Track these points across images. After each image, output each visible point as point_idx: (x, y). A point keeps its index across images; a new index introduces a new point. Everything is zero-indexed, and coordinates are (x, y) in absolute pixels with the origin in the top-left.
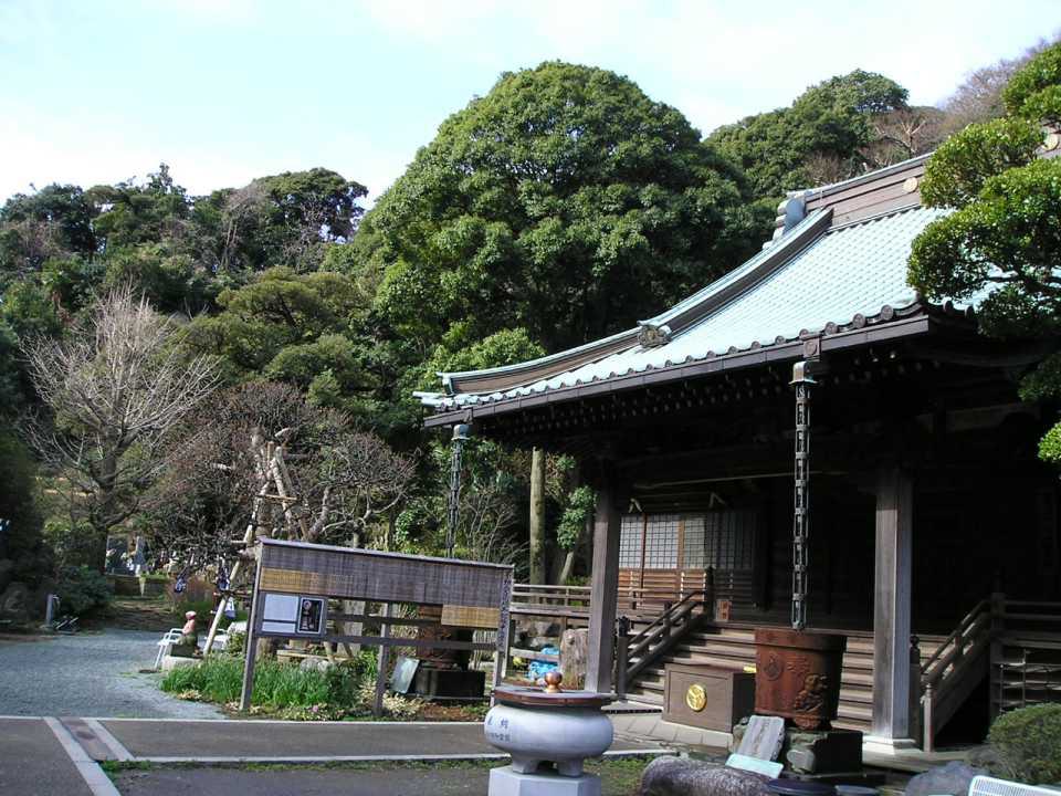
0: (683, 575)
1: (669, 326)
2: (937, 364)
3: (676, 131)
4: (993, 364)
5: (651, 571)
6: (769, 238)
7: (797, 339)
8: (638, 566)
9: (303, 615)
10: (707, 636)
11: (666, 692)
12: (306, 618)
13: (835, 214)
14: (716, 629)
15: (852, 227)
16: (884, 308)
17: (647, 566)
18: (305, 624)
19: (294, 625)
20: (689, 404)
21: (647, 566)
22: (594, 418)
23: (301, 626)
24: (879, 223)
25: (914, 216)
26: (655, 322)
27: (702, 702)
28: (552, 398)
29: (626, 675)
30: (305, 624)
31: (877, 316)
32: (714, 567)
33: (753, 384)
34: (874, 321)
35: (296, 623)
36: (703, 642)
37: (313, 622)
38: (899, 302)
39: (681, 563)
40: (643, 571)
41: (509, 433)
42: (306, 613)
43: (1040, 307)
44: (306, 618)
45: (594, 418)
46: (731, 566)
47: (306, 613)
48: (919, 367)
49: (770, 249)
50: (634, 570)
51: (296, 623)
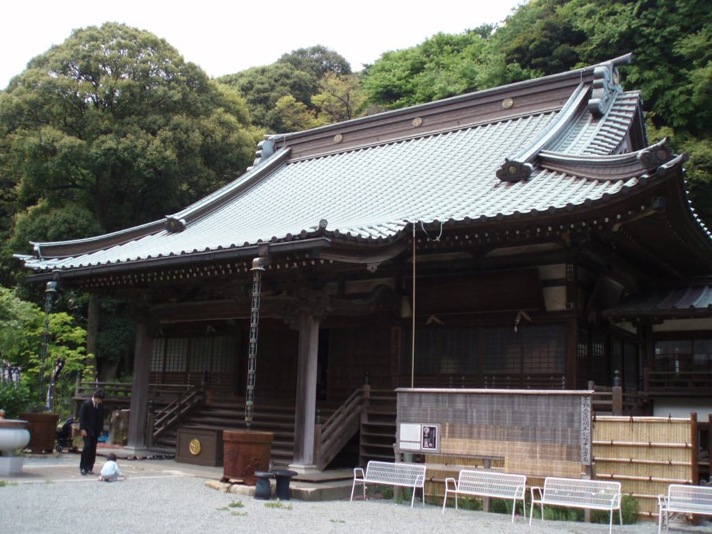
0: (189, 375)
1: (185, 219)
2: (331, 262)
3: (195, 78)
4: (362, 262)
5: (169, 373)
7: (256, 244)
8: (161, 370)
11: (177, 446)
13: (293, 152)
14: (208, 408)
17: (167, 370)
18: (426, 443)
20: (195, 275)
21: (167, 370)
22: (137, 281)
24: (318, 160)
26: (176, 216)
27: (199, 449)
28: (111, 269)
29: (153, 437)
30: (426, 443)
31: (299, 236)
32: (209, 370)
34: (297, 238)
36: (201, 416)
37: (431, 442)
38: (311, 228)
39: (188, 368)
40: (164, 372)
43: (641, 28)
45: (137, 281)
46: (219, 370)
48: (322, 262)
49: (252, 172)
50: (159, 373)
51: (420, 442)
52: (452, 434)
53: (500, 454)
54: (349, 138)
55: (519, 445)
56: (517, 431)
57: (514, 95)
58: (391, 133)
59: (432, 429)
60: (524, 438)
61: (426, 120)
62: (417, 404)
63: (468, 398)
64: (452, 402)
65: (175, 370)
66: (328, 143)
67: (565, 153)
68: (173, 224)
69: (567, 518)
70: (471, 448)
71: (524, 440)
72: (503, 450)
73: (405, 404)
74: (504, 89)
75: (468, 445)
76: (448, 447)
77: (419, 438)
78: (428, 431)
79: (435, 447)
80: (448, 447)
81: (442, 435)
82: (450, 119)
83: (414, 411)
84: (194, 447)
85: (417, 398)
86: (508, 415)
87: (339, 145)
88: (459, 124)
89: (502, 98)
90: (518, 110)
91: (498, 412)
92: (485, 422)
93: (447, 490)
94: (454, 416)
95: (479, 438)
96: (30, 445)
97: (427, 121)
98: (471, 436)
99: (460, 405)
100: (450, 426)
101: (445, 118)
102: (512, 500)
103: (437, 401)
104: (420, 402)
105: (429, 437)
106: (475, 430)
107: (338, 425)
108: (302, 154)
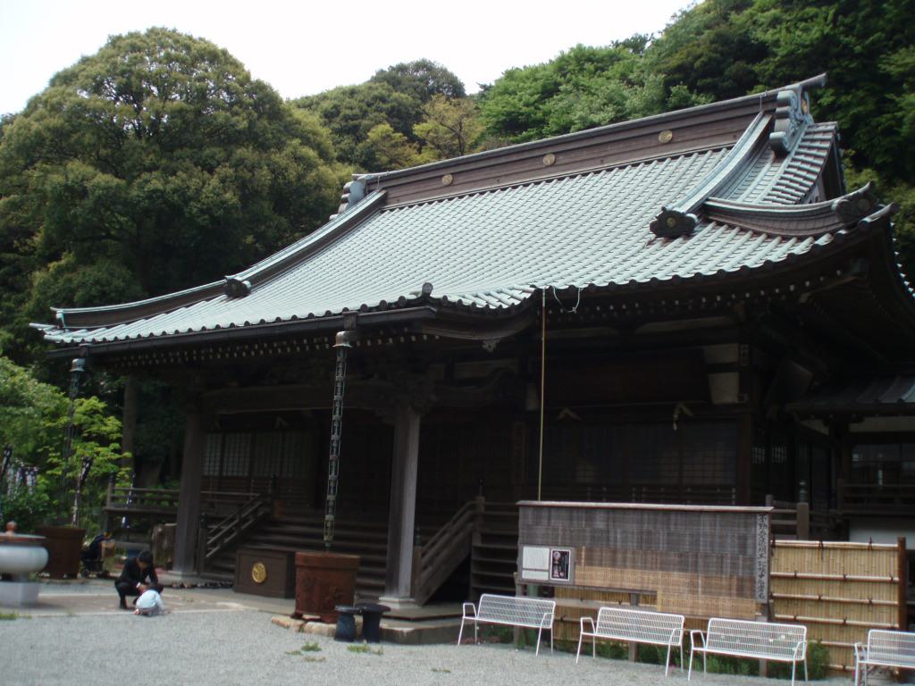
2: (437, 337)
6: (335, 211)
8: (217, 474)
9: (554, 565)
10: (273, 529)
12: (556, 567)
13: (390, 196)
15: (715, 151)
16: (424, 285)
19: (547, 573)
21: (224, 474)
22: (187, 359)
23: (553, 574)
25: (469, 201)
27: (264, 576)
28: (155, 343)
30: (556, 572)
33: (304, 338)
35: (548, 571)
36: (267, 533)
41: (116, 366)
42: (557, 562)
44: (556, 567)
45: (187, 359)
47: (557, 562)
48: (425, 337)
49: (337, 221)
52: (590, 561)
54: (461, 179)
55: (676, 576)
56: (673, 558)
59: (564, 554)
60: (683, 566)
61: (561, 157)
67: (739, 201)
72: (655, 582)
73: (530, 521)
79: (567, 578)
81: (577, 562)
83: (540, 530)
84: (258, 573)
85: (545, 513)
94: (593, 538)
95: (625, 567)
98: (613, 564)
99: (600, 524)
100: (587, 550)
101: (585, 155)
103: (571, 519)
104: (549, 519)
105: (560, 564)
106: (619, 556)
107: (444, 547)
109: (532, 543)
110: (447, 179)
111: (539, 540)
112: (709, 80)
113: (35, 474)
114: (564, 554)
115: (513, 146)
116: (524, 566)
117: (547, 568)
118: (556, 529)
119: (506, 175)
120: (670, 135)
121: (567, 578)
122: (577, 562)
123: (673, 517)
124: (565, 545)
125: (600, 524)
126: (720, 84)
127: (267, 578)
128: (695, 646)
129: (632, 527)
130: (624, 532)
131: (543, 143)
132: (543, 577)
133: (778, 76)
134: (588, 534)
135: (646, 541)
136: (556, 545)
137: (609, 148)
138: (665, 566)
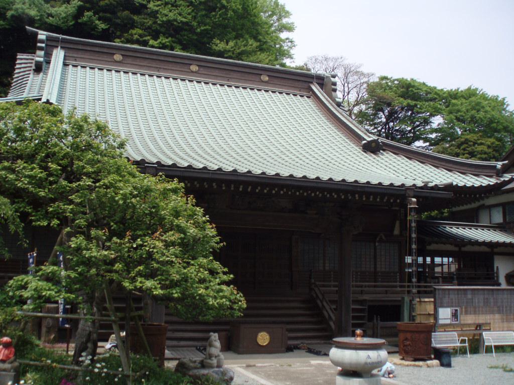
52: (466, 313)
53: (489, 321)
54: (129, 61)
55: (497, 316)
56: (496, 309)
57: (199, 63)
58: (171, 70)
59: (456, 310)
60: (499, 312)
61: (201, 69)
62: (447, 296)
63: (460, 292)
64: (466, 294)
65: (387, 270)
66: (105, 58)
67: (25, 95)
68: (373, 145)
69: (504, 351)
70: (476, 319)
71: (500, 313)
72: (490, 319)
73: (441, 296)
74: (153, 51)
75: (474, 318)
76: (464, 320)
77: (449, 316)
78: (454, 312)
79: (457, 321)
80: (464, 320)
81: (461, 313)
82: (205, 73)
83: (446, 300)
84: (263, 338)
85: (447, 292)
86: (492, 300)
87: (118, 64)
88: (228, 80)
89: (191, 63)
90: (271, 85)
91: (487, 299)
92: (482, 304)
93: (467, 345)
94: (467, 302)
95: (479, 314)
96: (362, 334)
97: (202, 71)
98: (475, 313)
99: (469, 296)
100: (465, 308)
101: (217, 73)
102: (491, 346)
103: (458, 294)
104: (449, 294)
105: (455, 315)
106: (477, 309)
107: (329, 315)
108: (77, 59)
109: (442, 306)
110: (118, 57)
111: (445, 305)
112: (108, 15)
113: (195, 271)
114: (456, 311)
115: (250, 63)
116: (440, 318)
117: (449, 317)
118: (452, 299)
119: (164, 69)
120: (267, 78)
121: (457, 321)
122: (461, 313)
123: (495, 292)
124: (456, 306)
125: (469, 296)
126: (114, 20)
127: (256, 340)
128: (466, 346)
129: (481, 297)
130: (478, 299)
131: (172, 54)
132: (448, 322)
133: (153, 28)
134: (465, 301)
135: (486, 302)
136: (453, 307)
137: (232, 73)
138: (492, 312)
